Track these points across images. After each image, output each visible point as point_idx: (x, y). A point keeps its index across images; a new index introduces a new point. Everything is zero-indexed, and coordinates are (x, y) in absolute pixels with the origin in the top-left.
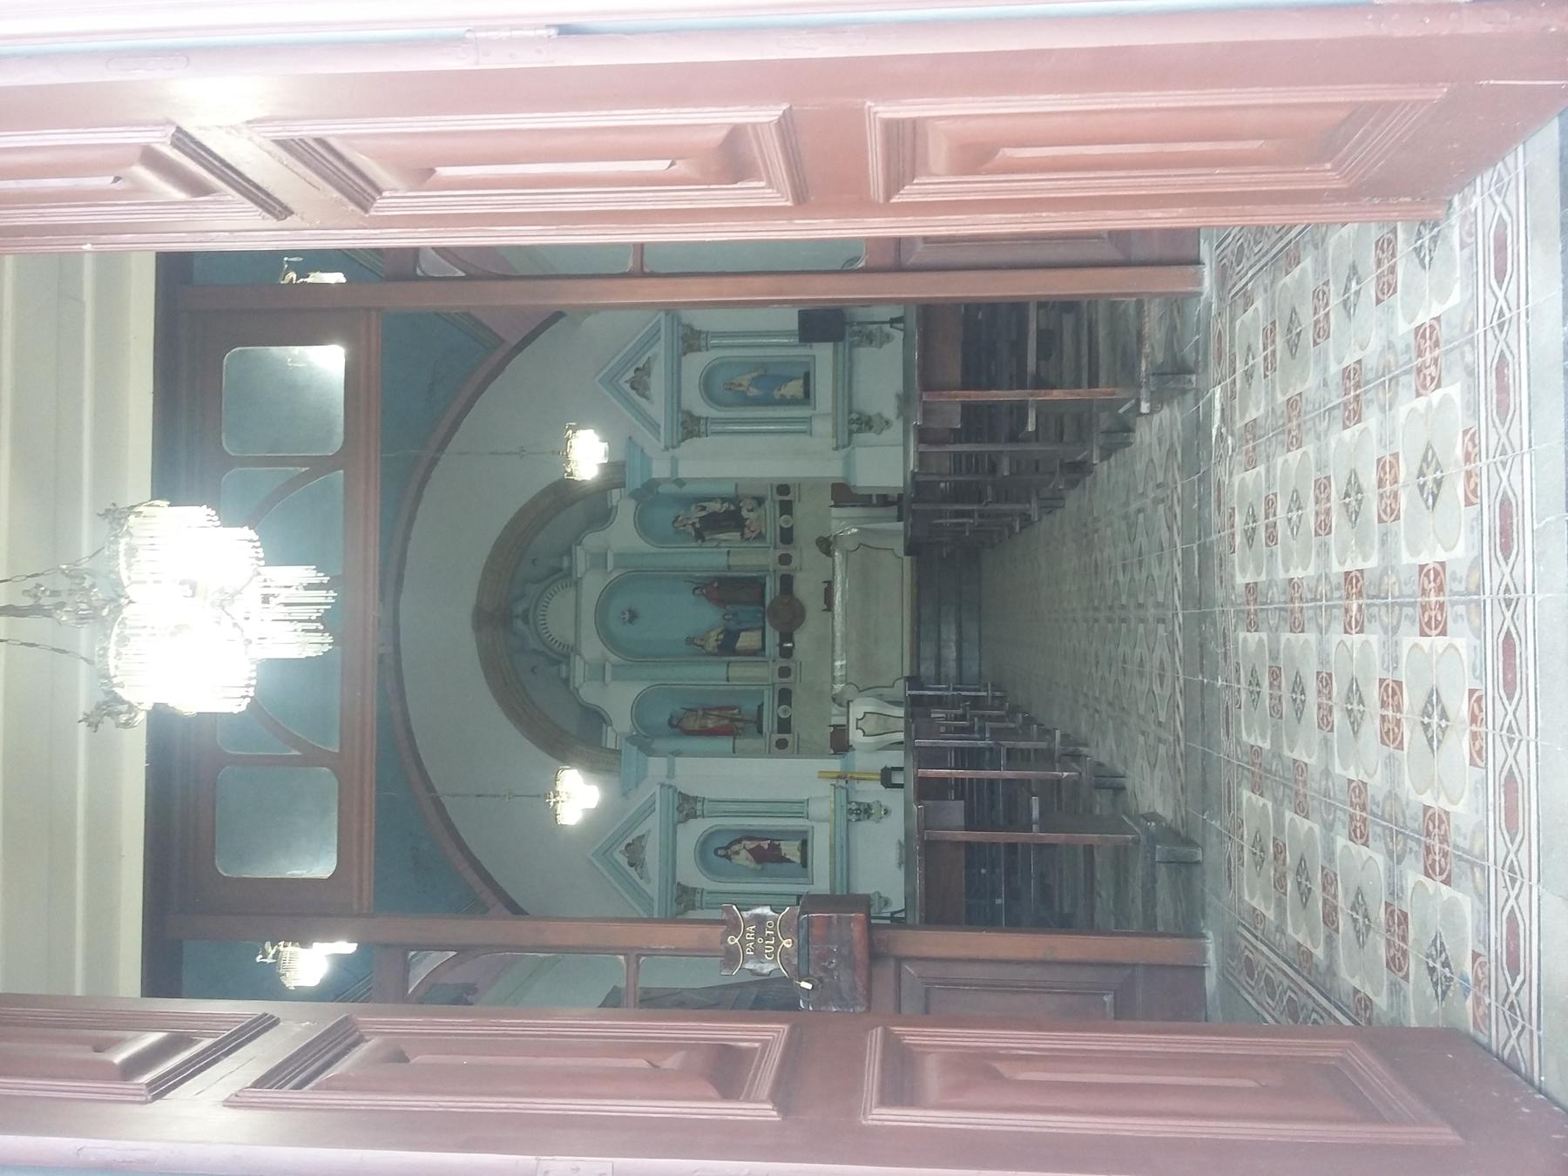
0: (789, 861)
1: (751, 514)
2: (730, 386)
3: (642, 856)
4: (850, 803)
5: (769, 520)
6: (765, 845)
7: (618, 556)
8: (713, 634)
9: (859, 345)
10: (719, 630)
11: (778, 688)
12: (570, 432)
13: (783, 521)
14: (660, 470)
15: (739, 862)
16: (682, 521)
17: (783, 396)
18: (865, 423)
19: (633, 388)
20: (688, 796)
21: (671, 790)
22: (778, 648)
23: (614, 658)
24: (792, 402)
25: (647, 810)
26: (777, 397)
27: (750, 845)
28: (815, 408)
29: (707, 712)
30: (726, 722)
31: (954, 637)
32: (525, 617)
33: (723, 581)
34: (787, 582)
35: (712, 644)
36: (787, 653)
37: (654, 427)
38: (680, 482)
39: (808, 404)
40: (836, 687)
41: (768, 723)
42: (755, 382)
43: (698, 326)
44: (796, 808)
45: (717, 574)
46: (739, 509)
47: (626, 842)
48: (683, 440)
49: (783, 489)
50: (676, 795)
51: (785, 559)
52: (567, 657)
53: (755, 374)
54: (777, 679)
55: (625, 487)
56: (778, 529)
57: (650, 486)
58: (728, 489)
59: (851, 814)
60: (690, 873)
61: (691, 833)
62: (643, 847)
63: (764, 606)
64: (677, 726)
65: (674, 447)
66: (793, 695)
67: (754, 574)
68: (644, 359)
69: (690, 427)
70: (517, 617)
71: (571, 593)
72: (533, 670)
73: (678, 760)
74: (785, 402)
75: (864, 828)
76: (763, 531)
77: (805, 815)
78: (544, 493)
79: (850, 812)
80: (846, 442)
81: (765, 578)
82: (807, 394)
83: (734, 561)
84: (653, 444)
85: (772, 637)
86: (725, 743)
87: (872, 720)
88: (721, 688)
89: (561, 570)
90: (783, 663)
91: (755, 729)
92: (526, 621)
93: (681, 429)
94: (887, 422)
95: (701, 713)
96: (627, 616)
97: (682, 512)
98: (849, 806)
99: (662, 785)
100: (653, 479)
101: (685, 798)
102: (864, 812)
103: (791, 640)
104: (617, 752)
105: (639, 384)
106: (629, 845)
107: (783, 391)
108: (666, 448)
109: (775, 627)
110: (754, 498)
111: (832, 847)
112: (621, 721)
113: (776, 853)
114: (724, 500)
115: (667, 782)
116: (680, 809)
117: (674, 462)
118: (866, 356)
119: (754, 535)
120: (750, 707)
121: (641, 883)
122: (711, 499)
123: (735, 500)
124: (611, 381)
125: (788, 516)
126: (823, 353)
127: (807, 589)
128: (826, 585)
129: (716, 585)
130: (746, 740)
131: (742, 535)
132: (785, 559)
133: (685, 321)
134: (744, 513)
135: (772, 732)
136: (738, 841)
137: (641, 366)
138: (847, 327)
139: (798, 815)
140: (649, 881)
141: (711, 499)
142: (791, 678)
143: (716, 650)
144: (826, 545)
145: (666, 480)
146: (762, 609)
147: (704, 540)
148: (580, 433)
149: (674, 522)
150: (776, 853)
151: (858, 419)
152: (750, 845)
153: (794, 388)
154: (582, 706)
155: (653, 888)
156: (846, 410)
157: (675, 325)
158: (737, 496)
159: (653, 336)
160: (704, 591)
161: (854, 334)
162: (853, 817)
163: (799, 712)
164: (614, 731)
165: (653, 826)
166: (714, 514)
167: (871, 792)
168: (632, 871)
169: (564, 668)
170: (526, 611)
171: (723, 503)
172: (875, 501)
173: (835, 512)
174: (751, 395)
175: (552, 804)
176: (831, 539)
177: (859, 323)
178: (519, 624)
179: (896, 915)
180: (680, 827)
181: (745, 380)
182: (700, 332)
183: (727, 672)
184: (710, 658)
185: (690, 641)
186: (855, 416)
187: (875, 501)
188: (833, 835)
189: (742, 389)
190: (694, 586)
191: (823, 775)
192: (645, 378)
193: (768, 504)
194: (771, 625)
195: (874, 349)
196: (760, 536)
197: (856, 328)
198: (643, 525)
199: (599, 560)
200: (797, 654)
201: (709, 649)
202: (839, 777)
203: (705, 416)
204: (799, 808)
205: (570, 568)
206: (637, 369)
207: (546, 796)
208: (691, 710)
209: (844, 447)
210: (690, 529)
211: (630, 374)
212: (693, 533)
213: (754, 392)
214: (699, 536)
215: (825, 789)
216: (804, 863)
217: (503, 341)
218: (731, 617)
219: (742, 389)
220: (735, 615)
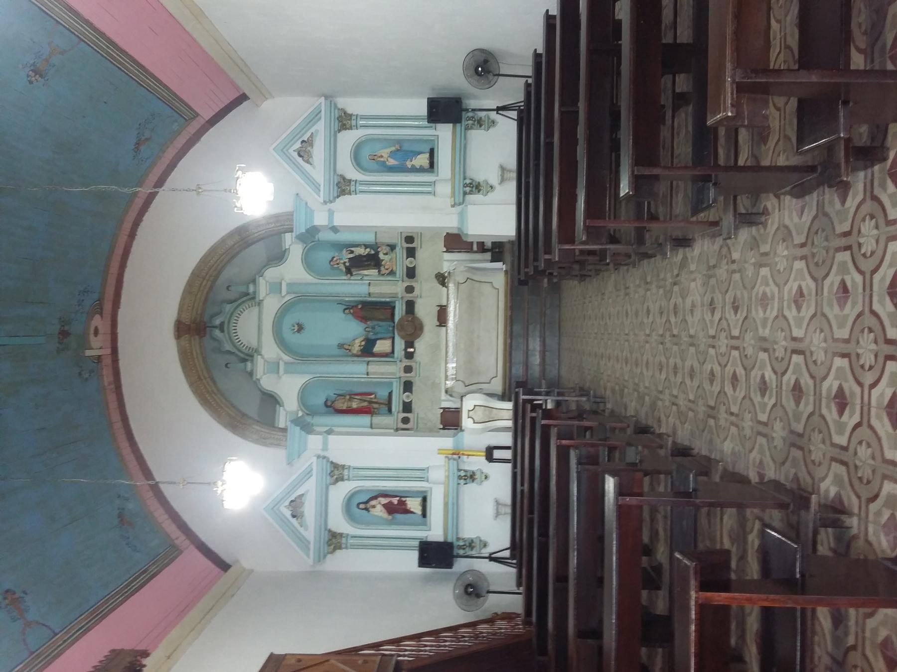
0: (412, 512)
1: (386, 256)
2: (373, 158)
3: (301, 510)
4: (459, 470)
5: (399, 261)
6: (395, 501)
7: (288, 285)
8: (357, 342)
9: (472, 128)
10: (362, 339)
11: (403, 380)
12: (240, 173)
13: (409, 262)
14: (320, 219)
15: (376, 514)
16: (336, 261)
17: (413, 165)
18: (475, 187)
19: (300, 156)
20: (338, 464)
21: (325, 460)
22: (403, 352)
23: (286, 358)
24: (421, 170)
25: (308, 474)
26: (410, 167)
27: (384, 501)
28: (438, 176)
29: (352, 396)
30: (365, 404)
31: (538, 348)
32: (221, 327)
33: (365, 304)
34: (410, 306)
35: (356, 349)
36: (409, 356)
37: (317, 188)
38: (335, 229)
39: (433, 172)
40: (447, 382)
41: (396, 406)
42: (392, 155)
43: (349, 111)
44: (418, 474)
45: (361, 299)
46: (377, 253)
47: (290, 499)
48: (338, 197)
49: (410, 239)
50: (329, 464)
51: (410, 290)
52: (252, 356)
53: (393, 149)
54: (402, 374)
55: (292, 232)
56: (401, 402)
57: (313, 231)
58: (369, 238)
59: (460, 479)
60: (339, 522)
61: (340, 493)
62: (303, 503)
63: (394, 323)
64: (330, 407)
65: (331, 202)
66: (414, 385)
67: (388, 300)
68: (309, 134)
69: (343, 187)
70: (215, 327)
71: (255, 310)
72: (226, 365)
73: (331, 438)
74: (414, 170)
75: (470, 489)
76: (394, 269)
77: (425, 479)
78: (231, 235)
79: (460, 477)
80: (461, 201)
81: (394, 302)
82: (432, 165)
83: (373, 290)
84: (315, 200)
85: (400, 344)
86: (365, 419)
87: (480, 411)
88: (363, 380)
89: (248, 294)
90: (407, 362)
91: (387, 408)
92: (222, 331)
93: (336, 188)
94: (492, 187)
95: (348, 397)
96: (296, 328)
97: (337, 254)
98: (459, 474)
99: (318, 457)
100: (314, 226)
101: (335, 466)
102: (470, 477)
103: (412, 346)
104: (284, 430)
105: (304, 153)
106: (292, 501)
107: (414, 162)
108: (325, 203)
109: (402, 337)
110: (388, 245)
111: (446, 504)
112: (290, 403)
113: (404, 507)
114: (366, 246)
115: (322, 454)
116: (331, 474)
117: (331, 213)
118: (477, 136)
119: (387, 272)
120: (383, 394)
121: (301, 530)
122: (358, 246)
123: (375, 246)
124: (283, 150)
125: (412, 259)
126: (444, 132)
127: (425, 311)
128: (439, 308)
129: (360, 306)
130: (380, 418)
131: (379, 271)
132: (410, 290)
133: (340, 106)
134: (381, 256)
135: (398, 412)
136: (375, 498)
137: (306, 139)
138: (464, 113)
139: (421, 479)
140: (306, 529)
141: (358, 246)
142: (413, 374)
143: (360, 353)
144: (442, 279)
145: (324, 227)
146: (392, 324)
147: (352, 275)
148: (249, 175)
149: (331, 261)
150: (404, 507)
151: (471, 184)
152: (384, 501)
153: (422, 160)
154: (261, 391)
155: (310, 534)
156: (462, 176)
157: (333, 109)
158: (376, 243)
159: (315, 117)
160: (352, 311)
161: (469, 119)
162: (462, 482)
163: (417, 398)
164: (285, 410)
165: (310, 488)
166: (360, 256)
167: (477, 463)
168: (294, 521)
169: (249, 364)
170: (222, 324)
171: (365, 249)
172: (475, 248)
173: (447, 256)
174: (390, 164)
175: (219, 492)
176: (446, 275)
177: (473, 110)
178: (217, 332)
179: (493, 556)
180: (331, 488)
181: (385, 152)
182: (351, 115)
183: (367, 369)
184: (355, 359)
185: (341, 346)
186: (468, 181)
187: (475, 248)
188: (446, 496)
189: (382, 159)
190: (345, 307)
191: (441, 451)
192: (309, 148)
193: (398, 249)
194: (399, 335)
195: (482, 131)
196: (392, 273)
197: (470, 114)
198: (308, 262)
199: (276, 288)
200: (417, 357)
201: (355, 352)
202: (453, 454)
203: (355, 179)
204: (421, 473)
205: (255, 292)
206: (303, 141)
207: (215, 483)
208: (339, 395)
209: (460, 204)
210: (342, 267)
211: (298, 145)
212: (344, 270)
213: (392, 162)
214: (349, 271)
215: (441, 460)
216: (424, 515)
217: (197, 115)
218: (370, 329)
219: (382, 159)
220: (373, 328)
